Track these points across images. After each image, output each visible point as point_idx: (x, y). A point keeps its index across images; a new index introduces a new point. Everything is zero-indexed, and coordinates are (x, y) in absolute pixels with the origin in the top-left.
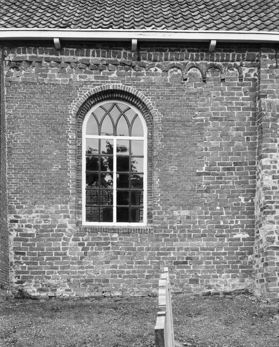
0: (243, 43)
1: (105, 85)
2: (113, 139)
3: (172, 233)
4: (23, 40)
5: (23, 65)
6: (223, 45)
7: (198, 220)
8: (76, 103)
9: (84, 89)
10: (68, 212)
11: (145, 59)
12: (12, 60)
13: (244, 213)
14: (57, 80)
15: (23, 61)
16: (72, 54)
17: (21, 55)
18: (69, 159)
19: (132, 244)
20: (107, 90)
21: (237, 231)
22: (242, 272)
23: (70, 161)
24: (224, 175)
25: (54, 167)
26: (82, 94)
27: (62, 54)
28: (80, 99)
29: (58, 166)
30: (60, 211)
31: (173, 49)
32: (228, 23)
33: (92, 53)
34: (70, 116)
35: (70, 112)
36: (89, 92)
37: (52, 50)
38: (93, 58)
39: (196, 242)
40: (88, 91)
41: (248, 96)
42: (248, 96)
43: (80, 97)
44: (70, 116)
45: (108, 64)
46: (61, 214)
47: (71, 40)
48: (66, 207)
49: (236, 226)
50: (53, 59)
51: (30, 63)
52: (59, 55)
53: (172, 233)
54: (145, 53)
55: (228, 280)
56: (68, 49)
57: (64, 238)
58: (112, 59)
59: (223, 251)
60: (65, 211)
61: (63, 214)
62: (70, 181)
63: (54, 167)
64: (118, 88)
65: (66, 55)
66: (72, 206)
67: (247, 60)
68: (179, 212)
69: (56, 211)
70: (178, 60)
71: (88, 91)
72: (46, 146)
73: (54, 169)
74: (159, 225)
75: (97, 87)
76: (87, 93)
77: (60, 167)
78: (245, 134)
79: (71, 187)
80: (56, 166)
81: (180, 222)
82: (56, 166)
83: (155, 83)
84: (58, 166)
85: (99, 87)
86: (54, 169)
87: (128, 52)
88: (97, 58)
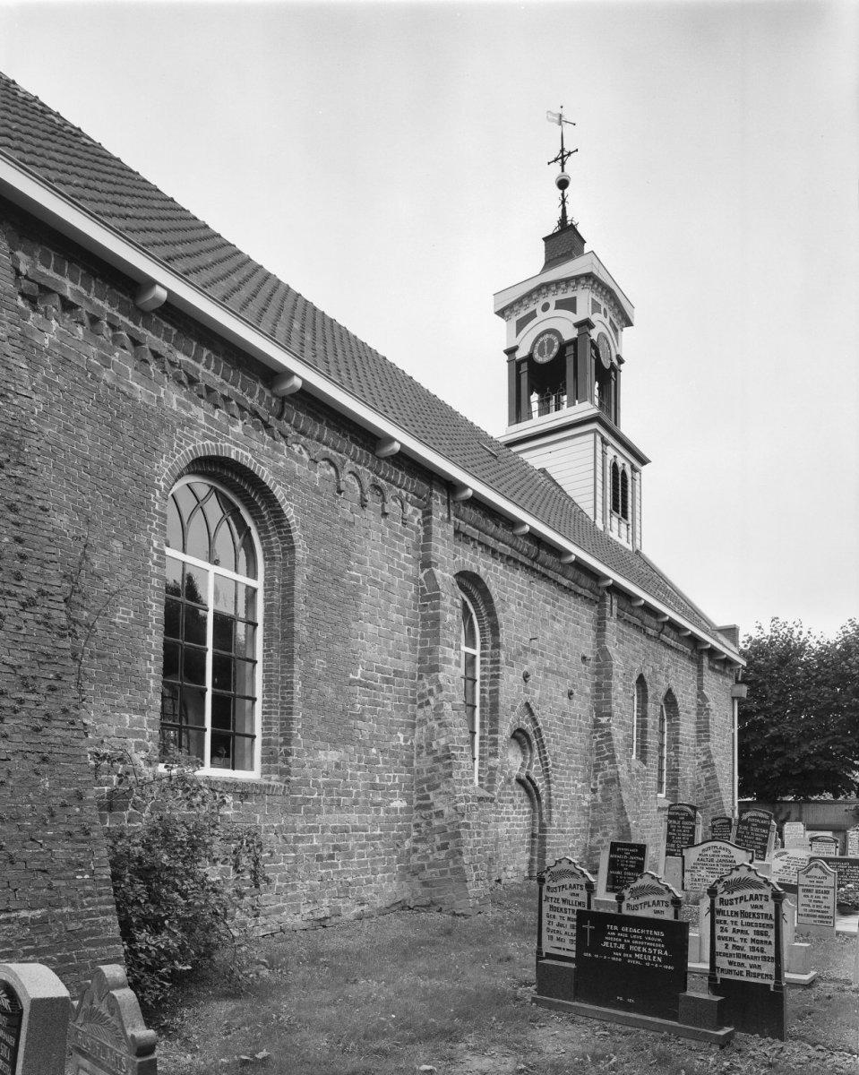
0: (233, 345)
1: (223, 445)
2: (208, 571)
3: (316, 796)
4: (355, 425)
5: (54, 305)
6: (406, 461)
7: (350, 772)
8: (170, 465)
9: (185, 436)
10: (144, 737)
11: (289, 421)
12: (24, 273)
13: (402, 763)
14: (132, 387)
15: (54, 292)
16: (167, 339)
17: (50, 273)
18: (152, 600)
19: (255, 818)
20: (225, 457)
21: (394, 795)
22: (400, 868)
23: (154, 604)
24: (382, 690)
25: (120, 614)
26: (181, 447)
27: (146, 327)
28: (178, 456)
29: (128, 614)
30: (128, 732)
31: (332, 424)
32: (92, 186)
33: (206, 358)
34: (157, 492)
35: (156, 482)
36: (194, 447)
37: (128, 303)
38: (207, 370)
39: (346, 816)
40: (193, 445)
41: (410, 556)
42: (410, 556)
43: (179, 452)
44: (157, 492)
45: (231, 400)
46: (130, 740)
47: (349, 416)
48: (140, 723)
49: (392, 787)
50: (128, 329)
51: (68, 306)
52: (140, 325)
53: (316, 796)
54: (293, 413)
55: (383, 885)
56: (162, 321)
57: (134, 802)
58: (237, 391)
59: (378, 832)
60: (138, 732)
61: (135, 740)
62: (153, 656)
63: (120, 614)
64: (244, 462)
65: (153, 334)
66: (154, 721)
67: (415, 494)
68: (326, 755)
69: (119, 731)
70: (334, 449)
71: (193, 445)
72: (103, 551)
73: (120, 618)
74: (299, 778)
75: (208, 442)
76: (191, 448)
77: (132, 616)
78: (407, 623)
79: (153, 673)
80: (124, 612)
81: (327, 773)
82: (124, 612)
83: (300, 478)
84: (128, 614)
85: (213, 444)
86: (120, 618)
87: (267, 393)
88: (213, 375)
